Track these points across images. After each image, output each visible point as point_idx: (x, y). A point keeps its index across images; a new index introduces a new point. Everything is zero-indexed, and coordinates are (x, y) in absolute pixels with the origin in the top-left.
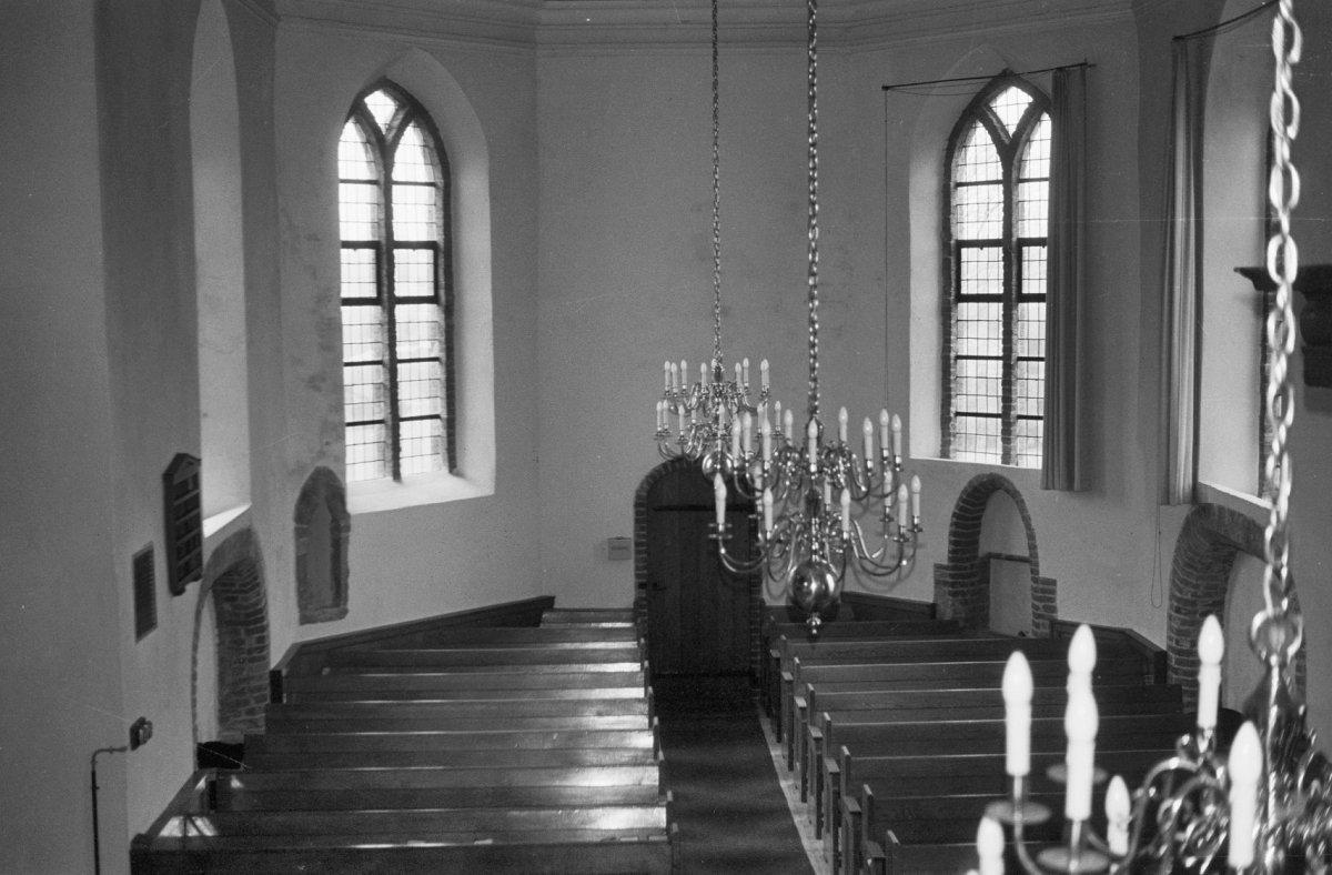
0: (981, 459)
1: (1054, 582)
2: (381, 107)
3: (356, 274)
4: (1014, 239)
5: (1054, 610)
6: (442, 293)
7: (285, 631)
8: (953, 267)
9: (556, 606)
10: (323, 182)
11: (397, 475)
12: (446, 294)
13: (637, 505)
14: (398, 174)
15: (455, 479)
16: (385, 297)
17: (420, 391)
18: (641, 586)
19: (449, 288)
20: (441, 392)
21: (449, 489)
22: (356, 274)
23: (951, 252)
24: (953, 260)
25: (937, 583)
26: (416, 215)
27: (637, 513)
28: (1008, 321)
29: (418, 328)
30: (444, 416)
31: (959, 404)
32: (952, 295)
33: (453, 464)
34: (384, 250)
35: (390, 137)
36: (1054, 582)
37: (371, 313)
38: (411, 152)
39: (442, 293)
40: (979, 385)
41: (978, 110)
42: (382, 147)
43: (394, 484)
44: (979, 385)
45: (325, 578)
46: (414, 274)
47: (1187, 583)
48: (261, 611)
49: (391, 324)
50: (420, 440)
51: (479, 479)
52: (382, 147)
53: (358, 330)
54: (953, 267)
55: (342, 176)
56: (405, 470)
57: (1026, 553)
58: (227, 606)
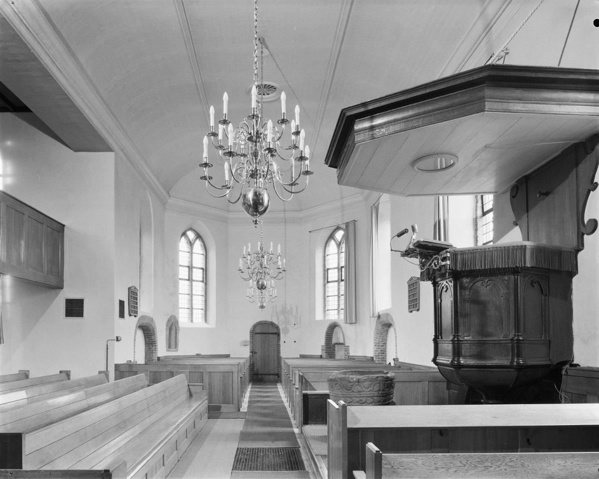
0: (333, 318)
1: (349, 346)
2: (191, 235)
3: (183, 273)
4: (340, 266)
5: (349, 353)
6: (204, 280)
7: (162, 351)
8: (326, 275)
9: (231, 356)
10: (175, 250)
11: (192, 321)
12: (205, 280)
13: (250, 332)
14: (194, 251)
15: (207, 324)
16: (190, 279)
17: (198, 302)
18: (251, 352)
19: (206, 279)
20: (204, 303)
21: (205, 325)
22: (183, 273)
23: (326, 271)
24: (326, 273)
25: (322, 350)
26: (199, 261)
27: (251, 334)
28: (339, 285)
29: (198, 288)
30: (204, 309)
31: (327, 308)
32: (326, 281)
33: (206, 321)
34: (190, 268)
35: (192, 242)
36: (349, 346)
37: (187, 283)
38: (198, 244)
39: (204, 280)
40: (332, 303)
41: (331, 236)
42: (191, 244)
43: (200, 177)
44: (332, 303)
45: (172, 343)
46: (198, 275)
47: (379, 358)
48: (155, 341)
49: (192, 285)
50: (198, 315)
51: (212, 323)
52: (191, 244)
53: (183, 286)
54: (326, 275)
55: (180, 249)
56: (194, 320)
57: (342, 342)
58: (147, 340)
